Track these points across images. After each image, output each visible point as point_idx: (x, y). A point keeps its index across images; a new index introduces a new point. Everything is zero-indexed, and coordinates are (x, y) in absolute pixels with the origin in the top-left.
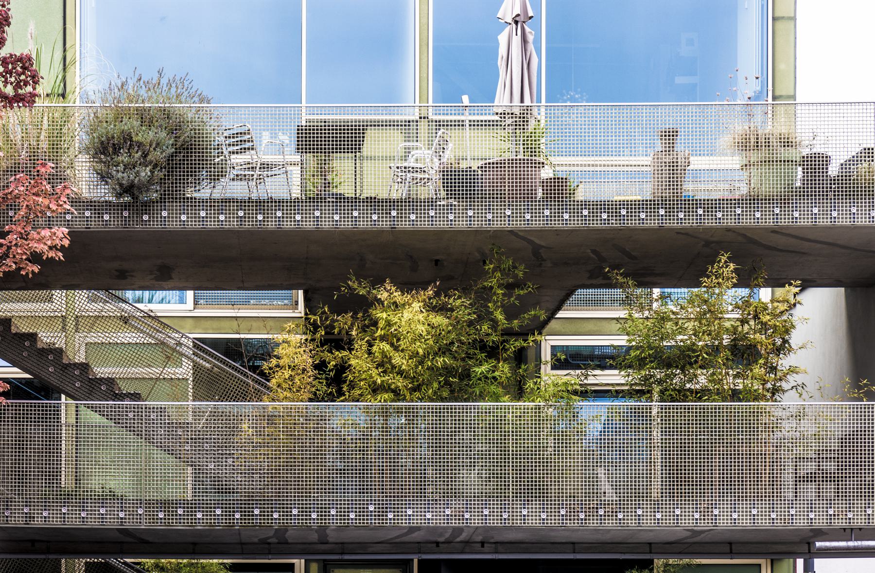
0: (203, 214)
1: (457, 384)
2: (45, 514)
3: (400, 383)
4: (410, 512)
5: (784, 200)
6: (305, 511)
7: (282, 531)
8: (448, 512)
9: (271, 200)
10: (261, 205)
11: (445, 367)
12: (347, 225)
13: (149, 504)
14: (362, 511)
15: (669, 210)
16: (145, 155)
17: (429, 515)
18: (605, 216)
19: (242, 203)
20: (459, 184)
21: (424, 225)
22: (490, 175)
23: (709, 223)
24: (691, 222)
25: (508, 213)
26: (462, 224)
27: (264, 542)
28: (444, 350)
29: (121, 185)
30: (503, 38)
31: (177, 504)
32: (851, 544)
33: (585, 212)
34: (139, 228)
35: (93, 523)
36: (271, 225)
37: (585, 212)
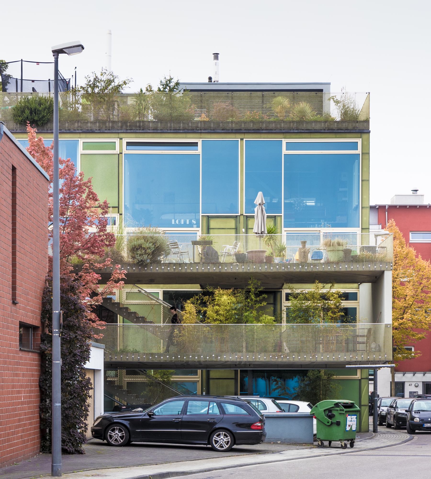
0: (163, 267)
2: (116, 357)
3: (222, 318)
4: (225, 357)
5: (337, 263)
7: (187, 362)
8: (236, 357)
10: (180, 265)
11: (235, 313)
12: (206, 271)
13: (147, 354)
14: (211, 356)
15: (303, 266)
17: (375, 267)
18: (283, 268)
19: (175, 264)
20: (240, 258)
21: (230, 271)
22: (250, 255)
23: (315, 270)
24: (309, 270)
25: (254, 267)
26: (241, 271)
27: (182, 365)
29: (138, 261)
30: (256, 209)
31: (155, 354)
32: (356, 366)
33: (278, 267)
35: (130, 360)
36: (183, 271)
37: (278, 267)
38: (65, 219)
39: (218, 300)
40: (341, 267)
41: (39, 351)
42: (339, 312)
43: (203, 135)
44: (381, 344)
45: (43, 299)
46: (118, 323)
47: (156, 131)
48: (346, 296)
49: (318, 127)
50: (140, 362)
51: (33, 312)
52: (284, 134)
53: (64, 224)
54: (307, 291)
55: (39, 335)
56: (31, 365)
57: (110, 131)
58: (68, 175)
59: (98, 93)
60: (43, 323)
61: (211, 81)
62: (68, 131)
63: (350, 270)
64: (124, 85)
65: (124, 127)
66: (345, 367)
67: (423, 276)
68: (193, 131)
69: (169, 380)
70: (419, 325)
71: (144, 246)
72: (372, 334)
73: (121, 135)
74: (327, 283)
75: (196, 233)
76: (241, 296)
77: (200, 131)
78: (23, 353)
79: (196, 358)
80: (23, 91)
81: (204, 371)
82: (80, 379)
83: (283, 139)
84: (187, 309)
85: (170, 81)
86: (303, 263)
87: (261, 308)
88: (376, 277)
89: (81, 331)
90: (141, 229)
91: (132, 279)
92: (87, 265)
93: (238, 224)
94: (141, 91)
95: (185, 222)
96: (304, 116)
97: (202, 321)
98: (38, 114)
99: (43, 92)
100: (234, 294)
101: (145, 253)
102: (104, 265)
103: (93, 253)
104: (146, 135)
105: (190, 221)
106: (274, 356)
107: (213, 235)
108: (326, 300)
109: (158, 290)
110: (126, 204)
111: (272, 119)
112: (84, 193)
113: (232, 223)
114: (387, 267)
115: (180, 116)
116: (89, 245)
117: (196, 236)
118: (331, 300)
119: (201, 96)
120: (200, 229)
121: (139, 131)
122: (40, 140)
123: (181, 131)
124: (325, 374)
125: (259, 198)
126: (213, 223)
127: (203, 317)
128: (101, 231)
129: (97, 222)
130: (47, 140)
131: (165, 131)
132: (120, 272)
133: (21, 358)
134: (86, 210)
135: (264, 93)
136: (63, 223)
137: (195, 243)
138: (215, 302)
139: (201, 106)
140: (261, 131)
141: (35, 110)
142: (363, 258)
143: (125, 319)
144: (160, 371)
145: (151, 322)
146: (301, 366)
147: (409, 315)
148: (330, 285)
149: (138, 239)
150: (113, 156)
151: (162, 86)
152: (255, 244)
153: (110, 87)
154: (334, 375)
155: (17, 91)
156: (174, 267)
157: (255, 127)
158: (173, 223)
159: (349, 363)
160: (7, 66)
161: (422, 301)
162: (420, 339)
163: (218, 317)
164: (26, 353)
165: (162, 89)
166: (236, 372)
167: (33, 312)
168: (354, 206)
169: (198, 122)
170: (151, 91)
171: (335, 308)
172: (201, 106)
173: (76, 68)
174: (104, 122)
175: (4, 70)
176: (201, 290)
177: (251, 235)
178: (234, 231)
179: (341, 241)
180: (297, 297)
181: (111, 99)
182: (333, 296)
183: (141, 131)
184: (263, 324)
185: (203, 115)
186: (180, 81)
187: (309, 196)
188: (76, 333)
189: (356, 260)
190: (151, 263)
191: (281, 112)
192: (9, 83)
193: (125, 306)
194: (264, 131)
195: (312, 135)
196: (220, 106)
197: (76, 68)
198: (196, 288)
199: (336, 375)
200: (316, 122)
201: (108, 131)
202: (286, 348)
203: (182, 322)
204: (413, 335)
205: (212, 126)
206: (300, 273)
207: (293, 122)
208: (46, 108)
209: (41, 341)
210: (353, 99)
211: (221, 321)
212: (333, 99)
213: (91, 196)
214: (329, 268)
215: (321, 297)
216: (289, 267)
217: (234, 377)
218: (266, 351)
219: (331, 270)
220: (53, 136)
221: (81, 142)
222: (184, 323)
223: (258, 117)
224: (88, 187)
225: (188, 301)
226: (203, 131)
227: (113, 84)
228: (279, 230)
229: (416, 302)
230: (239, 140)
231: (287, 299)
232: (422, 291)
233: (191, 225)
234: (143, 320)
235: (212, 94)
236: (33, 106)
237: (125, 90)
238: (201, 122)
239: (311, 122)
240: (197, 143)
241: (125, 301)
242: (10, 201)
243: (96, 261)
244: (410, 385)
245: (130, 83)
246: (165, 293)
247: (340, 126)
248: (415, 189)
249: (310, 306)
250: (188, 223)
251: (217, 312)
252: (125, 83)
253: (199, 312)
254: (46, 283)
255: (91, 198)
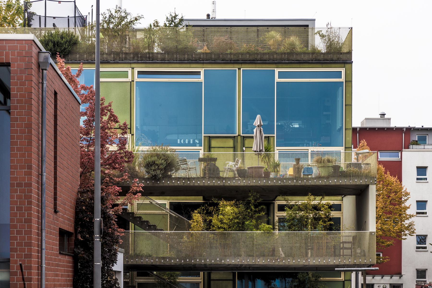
0: (174, 181)
1: (241, 227)
3: (225, 226)
4: (228, 260)
5: (328, 178)
6: (200, 260)
8: (238, 260)
9: (192, 178)
14: (216, 260)
15: (297, 181)
16: (158, 167)
18: (280, 182)
19: (184, 179)
20: (242, 173)
21: (232, 184)
25: (254, 181)
26: (242, 184)
28: (237, 218)
30: (255, 130)
32: (344, 269)
34: (156, 185)
35: (145, 263)
36: (192, 184)
38: (89, 139)
39: (223, 210)
40: (330, 182)
41: (73, 255)
42: (329, 221)
43: (205, 65)
44: (366, 250)
45: (76, 209)
46: (130, 231)
47: (163, 61)
48: (331, 207)
49: (306, 58)
50: (153, 265)
51: (69, 220)
52: (277, 64)
53: (88, 143)
54: (300, 203)
55: (73, 240)
56: (67, 267)
57: (123, 62)
58: (92, 100)
59: (113, 28)
60: (76, 230)
61: (209, 18)
62: (86, 62)
63: (339, 184)
64: (136, 21)
65: (136, 58)
66: (334, 270)
67: (391, 190)
68: (196, 62)
69: (175, 281)
70: (388, 233)
71: (157, 162)
72: (356, 241)
73: (133, 65)
74: (318, 196)
75: (199, 152)
76: (242, 207)
77: (202, 62)
78: (62, 256)
79: (203, 261)
80: (47, 27)
81: (206, 273)
82: (109, 279)
83: (276, 69)
84: (194, 218)
85: (175, 17)
86: (297, 177)
87: (259, 218)
88: (361, 190)
89: (110, 237)
90: (154, 148)
91: (148, 192)
92: (107, 179)
93: (236, 144)
94: (151, 26)
95: (189, 141)
96: (294, 48)
97: (207, 229)
98: (60, 46)
99: (62, 27)
100: (236, 205)
101: (158, 169)
102: (122, 180)
103: (114, 168)
104: (155, 65)
105: (194, 141)
106: (271, 260)
107: (214, 153)
108: (317, 211)
109: (165, 201)
110: (137, 126)
111: (266, 51)
112: (106, 115)
113: (230, 143)
114: (371, 181)
115: (185, 48)
116: (111, 161)
117: (199, 154)
118: (322, 211)
119: (204, 31)
120: (202, 148)
121: (148, 62)
122: (68, 69)
123: (186, 62)
124: (313, 277)
125: (258, 121)
126: (214, 143)
127: (209, 226)
128: (121, 149)
129: (117, 141)
130: (74, 69)
131: (171, 62)
132: (138, 185)
133: (60, 260)
134: (106, 131)
135: (259, 28)
136: (87, 142)
137: (201, 160)
138: (219, 212)
139: (204, 40)
140: (256, 62)
141: (58, 43)
142: (350, 173)
143: (136, 226)
144: (167, 273)
145: (162, 230)
146: (295, 268)
147: (380, 225)
148: (320, 197)
149: (152, 156)
150: (126, 83)
151: (168, 22)
152: (251, 161)
153: (123, 23)
154: (321, 277)
155: (40, 26)
156: (184, 181)
157: (252, 58)
158: (179, 142)
159: (338, 266)
160: (31, 5)
161: (390, 213)
162: (388, 245)
163: (222, 225)
164: (64, 256)
165: (168, 25)
166: (234, 274)
167: (69, 220)
168: (338, 127)
169: (200, 54)
170: (158, 26)
171: (325, 218)
172: (204, 40)
173: (92, 6)
174: (118, 54)
175: (29, 8)
176: (203, 201)
177: (248, 153)
178: (232, 149)
179: (330, 158)
180: (292, 208)
181: (124, 34)
182: (323, 207)
183: (150, 62)
184: (262, 231)
185: (205, 48)
186: (185, 18)
187: (295, 119)
188: (106, 239)
189: (344, 175)
190: (163, 178)
191: (273, 45)
192: (33, 19)
193: (138, 216)
194: (259, 62)
195: (301, 65)
196: (218, 40)
197: (92, 6)
198: (199, 200)
199: (323, 277)
200: (304, 53)
201: (122, 62)
202: (282, 253)
203: (190, 230)
204: (383, 243)
205: (213, 57)
206: (294, 186)
207: (285, 53)
208: (67, 41)
209: (75, 246)
210: (337, 34)
211: (224, 228)
212: (319, 33)
213: (112, 118)
214: (320, 182)
215: (313, 208)
216: (285, 181)
217: (232, 279)
218: (264, 256)
219: (321, 184)
220: (95, 66)
221: (277, 71)
222: (192, 230)
223: (253, 50)
224: (108, 110)
225: (196, 211)
226: (205, 62)
227: (126, 20)
228: (272, 149)
229: (385, 213)
230: (237, 69)
231: (279, 210)
232: (391, 204)
233: (194, 145)
234: (154, 228)
235: (213, 29)
236: (56, 39)
237: (137, 26)
238: (203, 53)
239: (300, 54)
240: (200, 72)
241: (138, 212)
242: (53, 122)
243: (115, 176)
244: (378, 287)
245: (141, 20)
246: (171, 204)
247: (326, 57)
248: (382, 113)
249: (304, 216)
250: (191, 142)
251: (221, 221)
252: (136, 19)
253: (205, 221)
254: (78, 194)
255: (112, 120)
